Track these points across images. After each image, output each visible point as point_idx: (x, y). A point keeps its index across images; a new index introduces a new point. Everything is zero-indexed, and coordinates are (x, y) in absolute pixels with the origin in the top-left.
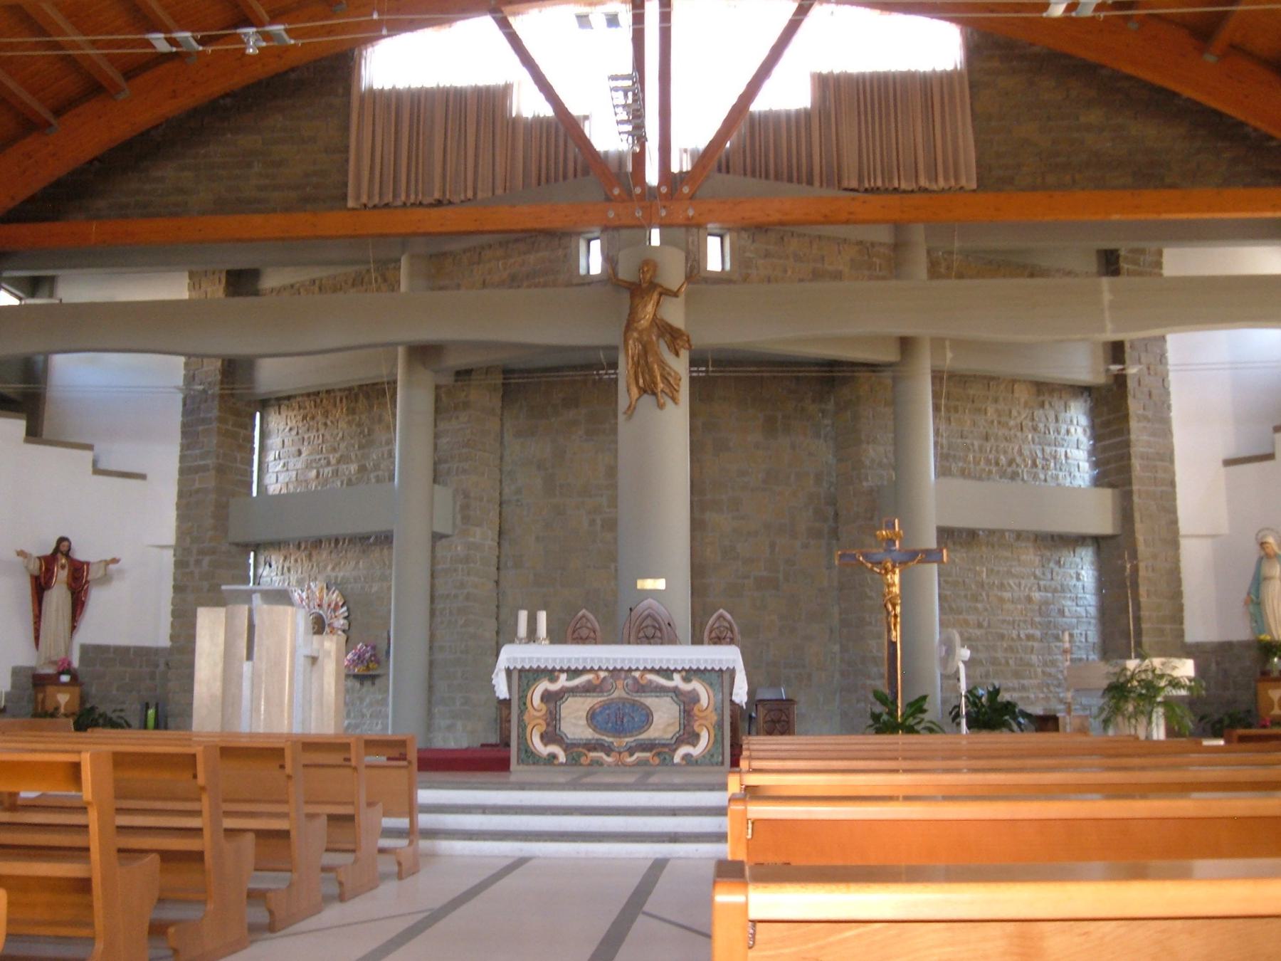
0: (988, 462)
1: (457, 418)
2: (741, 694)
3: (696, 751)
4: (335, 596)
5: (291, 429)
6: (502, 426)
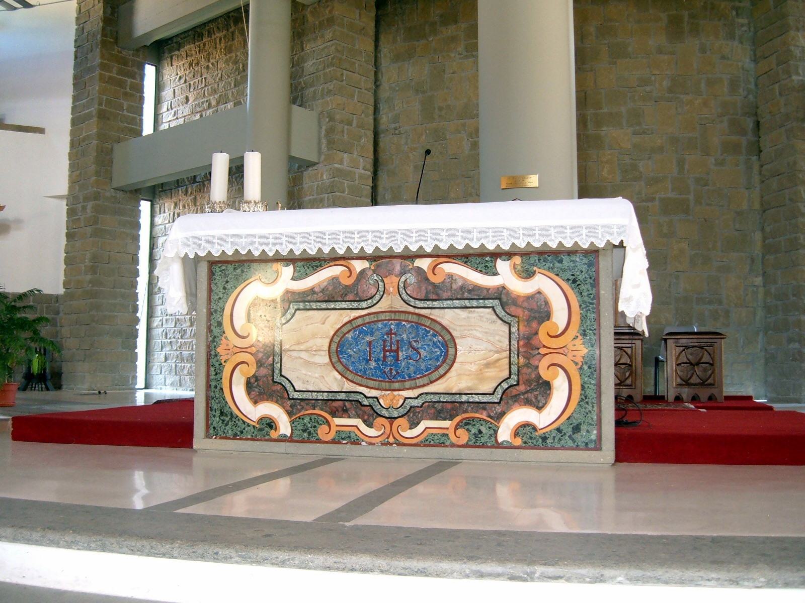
1: (322, 36)
2: (636, 298)
3: (543, 419)
5: (180, 78)
6: (377, 46)
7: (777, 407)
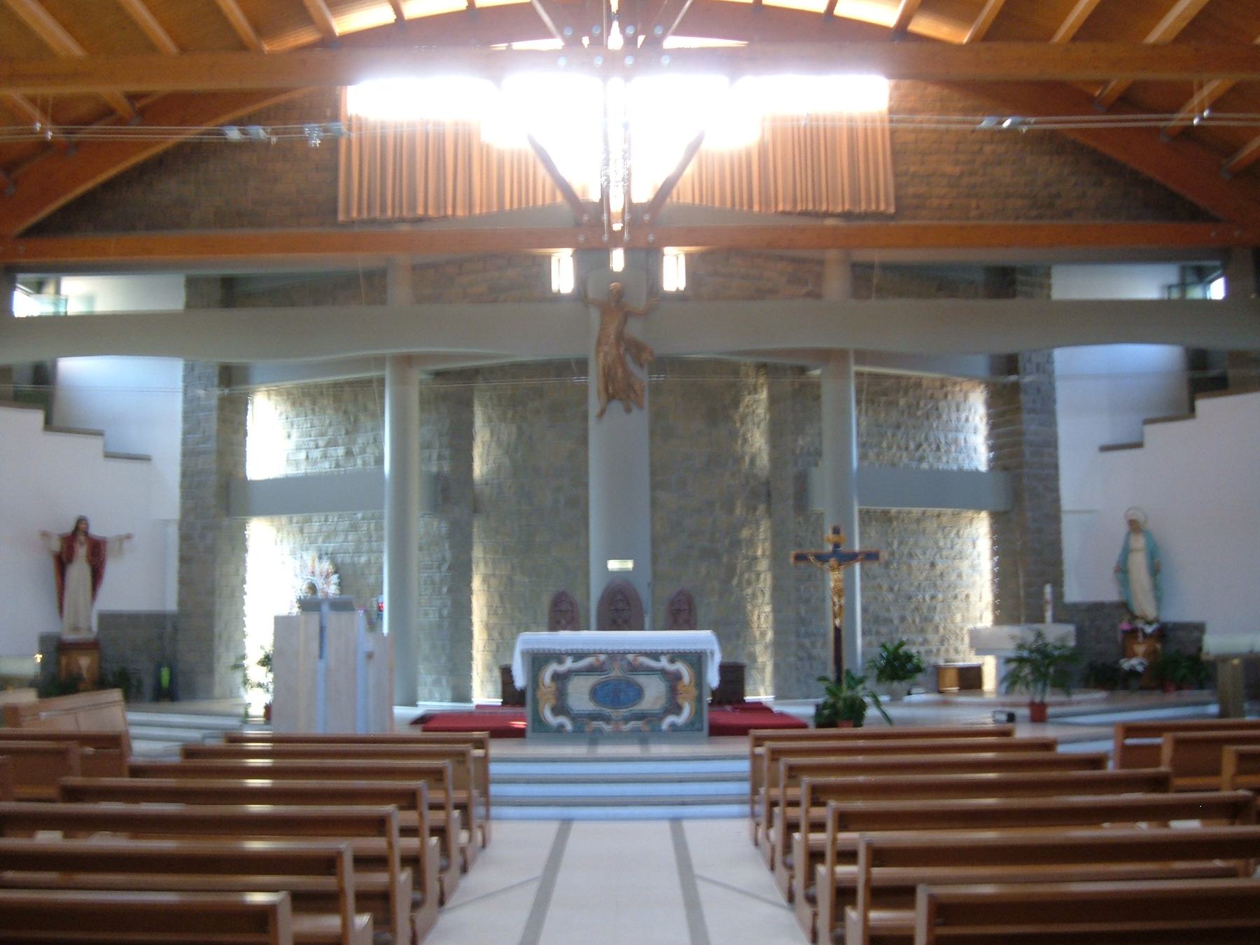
0: (899, 447)
4: (326, 566)
7: (776, 709)
